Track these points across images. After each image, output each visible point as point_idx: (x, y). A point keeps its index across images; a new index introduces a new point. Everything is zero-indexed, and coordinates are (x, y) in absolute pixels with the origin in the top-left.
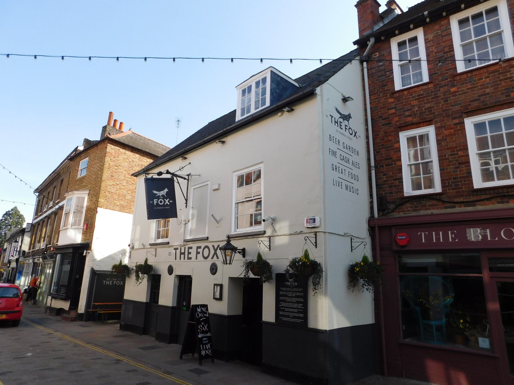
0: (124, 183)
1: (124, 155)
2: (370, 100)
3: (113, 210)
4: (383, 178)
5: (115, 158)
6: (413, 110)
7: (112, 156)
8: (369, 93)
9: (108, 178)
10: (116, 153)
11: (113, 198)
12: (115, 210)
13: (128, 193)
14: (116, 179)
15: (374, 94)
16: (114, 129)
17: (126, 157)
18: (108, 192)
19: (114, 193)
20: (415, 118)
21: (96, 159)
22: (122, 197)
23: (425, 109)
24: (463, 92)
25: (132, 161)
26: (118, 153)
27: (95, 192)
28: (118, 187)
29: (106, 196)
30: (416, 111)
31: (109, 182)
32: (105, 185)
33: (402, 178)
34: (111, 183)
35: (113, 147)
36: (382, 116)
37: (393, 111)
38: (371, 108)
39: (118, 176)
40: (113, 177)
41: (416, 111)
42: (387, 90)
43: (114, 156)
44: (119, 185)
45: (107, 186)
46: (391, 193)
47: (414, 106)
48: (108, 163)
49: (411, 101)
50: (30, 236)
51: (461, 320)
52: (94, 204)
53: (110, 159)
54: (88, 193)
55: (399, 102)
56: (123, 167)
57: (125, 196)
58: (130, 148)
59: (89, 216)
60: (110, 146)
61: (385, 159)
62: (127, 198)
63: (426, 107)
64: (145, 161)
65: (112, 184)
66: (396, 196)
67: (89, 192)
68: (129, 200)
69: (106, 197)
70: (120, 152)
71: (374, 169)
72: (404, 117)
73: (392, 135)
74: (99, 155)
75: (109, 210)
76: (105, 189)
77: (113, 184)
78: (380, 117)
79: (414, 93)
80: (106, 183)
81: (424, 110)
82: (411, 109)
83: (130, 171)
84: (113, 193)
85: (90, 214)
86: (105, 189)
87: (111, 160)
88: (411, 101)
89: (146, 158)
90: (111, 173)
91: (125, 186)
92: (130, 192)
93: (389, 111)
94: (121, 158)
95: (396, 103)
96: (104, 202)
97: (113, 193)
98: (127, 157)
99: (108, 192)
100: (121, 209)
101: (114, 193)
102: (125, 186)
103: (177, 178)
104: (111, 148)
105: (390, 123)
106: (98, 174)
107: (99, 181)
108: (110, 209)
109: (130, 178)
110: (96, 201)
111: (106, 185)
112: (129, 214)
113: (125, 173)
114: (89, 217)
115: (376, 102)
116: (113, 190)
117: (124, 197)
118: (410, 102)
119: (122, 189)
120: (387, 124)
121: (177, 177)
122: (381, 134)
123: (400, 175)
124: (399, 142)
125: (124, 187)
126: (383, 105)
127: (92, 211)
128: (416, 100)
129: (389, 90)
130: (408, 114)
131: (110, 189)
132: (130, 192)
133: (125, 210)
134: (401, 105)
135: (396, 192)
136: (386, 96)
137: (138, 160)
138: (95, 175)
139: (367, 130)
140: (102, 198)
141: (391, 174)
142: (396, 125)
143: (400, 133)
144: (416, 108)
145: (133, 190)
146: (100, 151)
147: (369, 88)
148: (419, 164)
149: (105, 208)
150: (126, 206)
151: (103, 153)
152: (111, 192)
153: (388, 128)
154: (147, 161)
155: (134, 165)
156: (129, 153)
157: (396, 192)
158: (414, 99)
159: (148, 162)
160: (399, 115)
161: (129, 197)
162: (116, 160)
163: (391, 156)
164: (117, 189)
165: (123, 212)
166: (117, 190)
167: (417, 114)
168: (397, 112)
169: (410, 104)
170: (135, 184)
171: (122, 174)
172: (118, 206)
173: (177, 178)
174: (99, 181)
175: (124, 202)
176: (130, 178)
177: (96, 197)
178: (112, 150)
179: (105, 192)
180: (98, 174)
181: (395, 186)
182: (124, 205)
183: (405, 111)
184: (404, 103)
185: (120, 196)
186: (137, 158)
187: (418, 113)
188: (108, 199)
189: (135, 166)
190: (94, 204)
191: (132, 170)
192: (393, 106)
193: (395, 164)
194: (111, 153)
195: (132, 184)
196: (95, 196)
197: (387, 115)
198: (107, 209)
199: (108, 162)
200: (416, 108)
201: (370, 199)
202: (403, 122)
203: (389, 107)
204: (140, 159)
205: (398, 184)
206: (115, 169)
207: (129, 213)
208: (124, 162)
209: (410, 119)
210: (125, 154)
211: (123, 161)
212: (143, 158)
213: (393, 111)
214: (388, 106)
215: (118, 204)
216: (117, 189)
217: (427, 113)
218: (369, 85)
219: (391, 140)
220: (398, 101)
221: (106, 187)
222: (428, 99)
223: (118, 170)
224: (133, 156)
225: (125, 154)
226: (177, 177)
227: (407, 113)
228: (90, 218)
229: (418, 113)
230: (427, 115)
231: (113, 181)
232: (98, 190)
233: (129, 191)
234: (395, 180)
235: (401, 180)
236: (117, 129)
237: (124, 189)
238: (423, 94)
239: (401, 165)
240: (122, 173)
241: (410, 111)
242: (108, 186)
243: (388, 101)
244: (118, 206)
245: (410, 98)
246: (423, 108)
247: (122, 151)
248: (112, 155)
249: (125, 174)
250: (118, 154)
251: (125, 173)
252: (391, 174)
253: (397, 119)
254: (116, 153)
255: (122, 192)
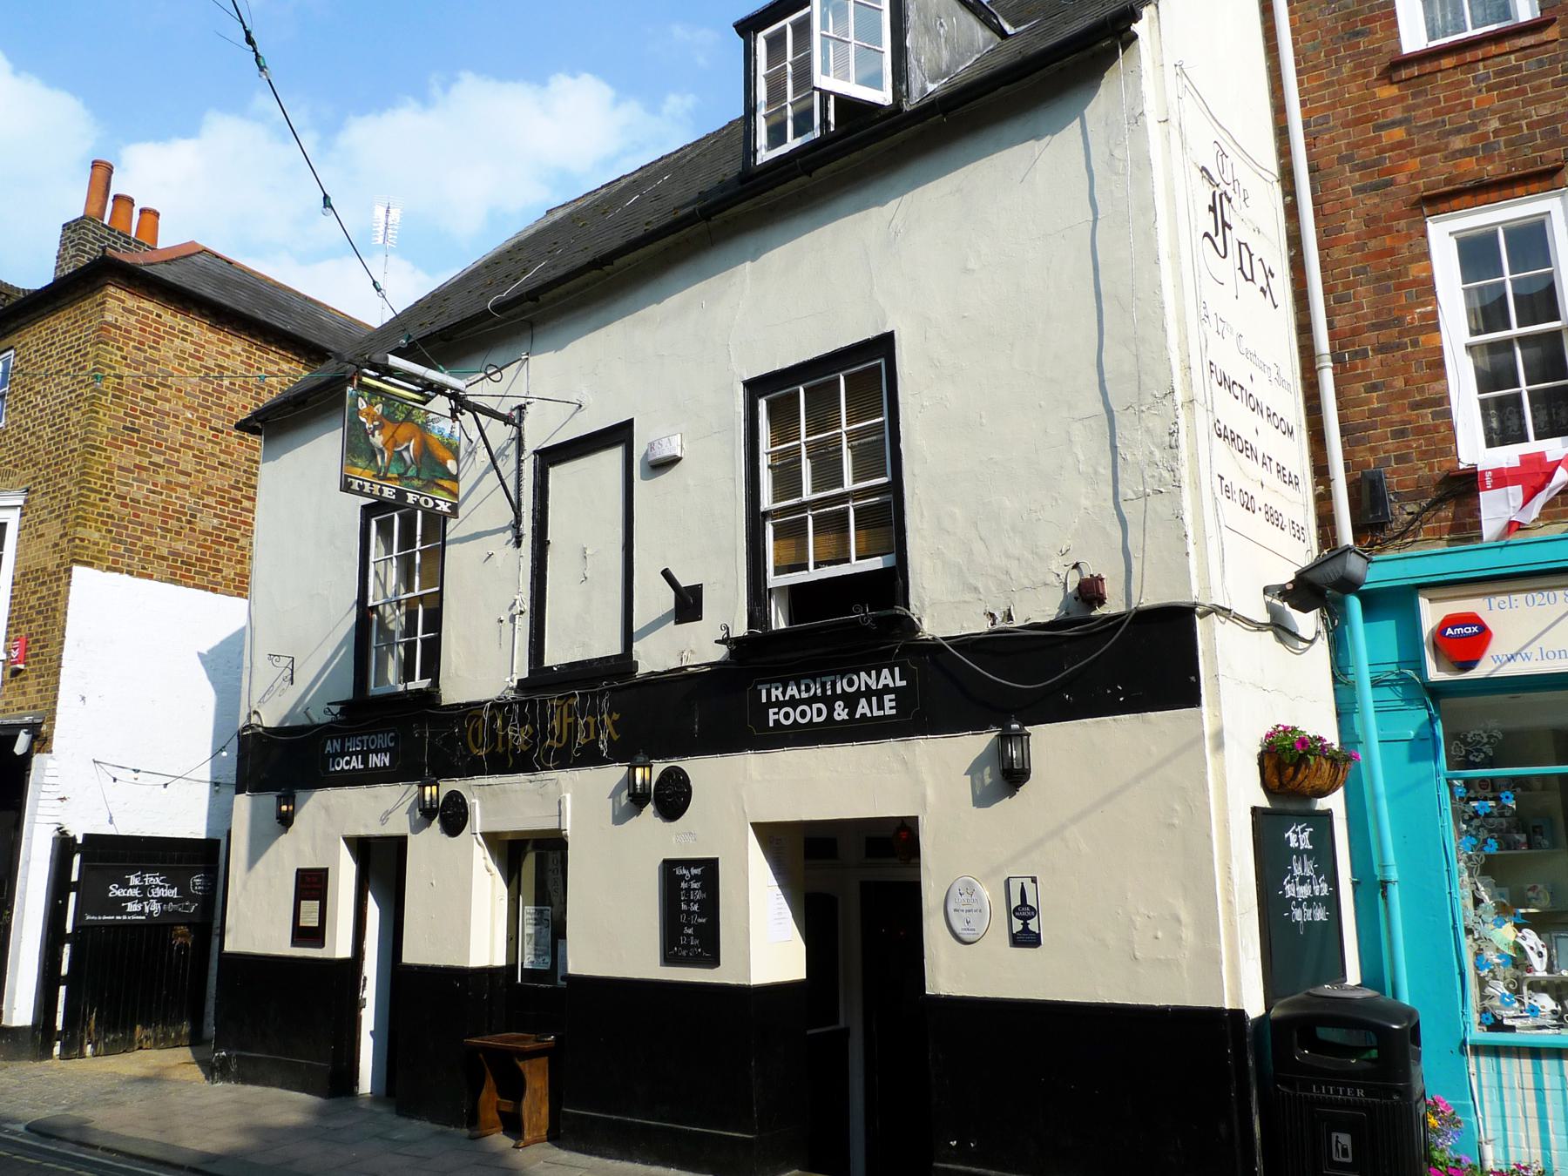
0: (187, 461)
1: (183, 339)
2: (1302, 92)
3: (140, 575)
4: (1368, 401)
5: (145, 352)
6: (1482, 129)
7: (132, 343)
8: (1297, 63)
9: (116, 439)
10: (145, 331)
11: (142, 524)
12: (150, 577)
13: (205, 505)
14: (152, 443)
15: (1315, 68)
16: (114, 236)
17: (190, 348)
18: (117, 496)
19: (145, 503)
20: (1491, 160)
21: (51, 356)
22: (179, 520)
23: (1529, 126)
24: (1455, 126)
25: (217, 369)
26: (157, 329)
27: (55, 497)
28: (161, 479)
29: (111, 517)
30: (1493, 132)
31: (123, 456)
32: (101, 468)
33: (1448, 397)
34: (125, 457)
35: (131, 302)
36: (1353, 154)
37: (1399, 134)
38: (1306, 125)
39: (158, 431)
40: (135, 435)
41: (1493, 132)
42: (1367, 52)
43: (140, 342)
44: (163, 467)
45: (112, 474)
46: (1400, 459)
47: (1483, 113)
48: (112, 372)
49: (1470, 94)
50: (886, 566)
51: (1285, 893)
52: (54, 552)
53: (119, 353)
54: (21, 502)
55: (1420, 100)
56: (180, 391)
57: (192, 516)
58: (207, 313)
59: (32, 603)
60: (119, 299)
61: (1373, 324)
62: (199, 526)
63: (1535, 118)
64: (273, 368)
65: (136, 466)
66: (1427, 470)
67: (26, 501)
68: (210, 534)
69: (110, 521)
70: (162, 328)
71: (1331, 365)
72: (1446, 158)
73: (1397, 231)
74: (68, 340)
75: (125, 576)
76: (105, 486)
77: (137, 462)
78: (1342, 160)
79: (1481, 64)
80: (109, 458)
81: (1525, 127)
82: (1473, 127)
83: (209, 408)
84: (139, 502)
85: (36, 596)
86: (105, 486)
87: (125, 358)
88: (1470, 94)
89: (275, 357)
90: (125, 414)
91: (189, 475)
92: (210, 500)
93: (1380, 136)
94: (167, 350)
95: (1411, 102)
96: (101, 542)
97: (139, 502)
98: (196, 350)
99: (117, 496)
100: (179, 572)
101: (145, 503)
102: (189, 475)
103: (476, 419)
104: (123, 308)
105: (1391, 183)
106: (67, 420)
107: (71, 451)
108: (130, 573)
109: (209, 441)
110: (61, 537)
111: (107, 468)
112: (210, 594)
113: (190, 416)
114: (30, 608)
115: (1323, 98)
116: (139, 488)
117: (189, 522)
118: (1466, 96)
119: (178, 484)
120: (1375, 187)
121: (478, 414)
122: (1353, 226)
123: (1437, 386)
124: (1426, 255)
125: (182, 479)
126: (1355, 110)
127: (44, 583)
128: (1490, 89)
129: (1379, 50)
130: (1462, 146)
131: (126, 484)
132: (210, 500)
133: (193, 578)
134: (1429, 109)
135: (1424, 455)
136: (1366, 75)
137: (242, 362)
138: (50, 427)
139: (1292, 211)
140: (94, 524)
141: (1399, 383)
142: (1415, 189)
143: (1435, 222)
144: (1495, 124)
145: (224, 491)
146: (73, 320)
147: (1294, 46)
148: (1507, 344)
149: (109, 569)
150: (197, 559)
151: (88, 328)
152: (132, 500)
153: (1377, 200)
154: (279, 370)
155: (226, 382)
156: (200, 331)
157: (1424, 455)
158: (1484, 84)
159: (283, 372)
160: (1425, 152)
161: (207, 521)
162: (145, 358)
163: (1396, 314)
164: (155, 485)
165: (186, 585)
166: (154, 492)
167: (1496, 146)
168: (1413, 139)
169: (1467, 106)
170: (231, 467)
171: (177, 423)
172: (164, 558)
173: (476, 419)
174: (71, 451)
175: (191, 543)
176: (209, 441)
177: (63, 521)
178: (128, 315)
179: (103, 496)
180: (67, 420)
181: (1420, 431)
182: (189, 557)
183: (1449, 135)
184: (1442, 104)
185: (171, 517)
186: (239, 355)
187: (1502, 143)
188: (118, 526)
189: (231, 390)
190: (54, 552)
191: (218, 405)
192: (1397, 113)
193: (1415, 343)
194: (126, 331)
195: (221, 464)
196: (58, 516)
197: (1374, 150)
198: (115, 570)
199: (113, 368)
200: (1491, 122)
201: (1317, 484)
202: (1443, 177)
203: (1381, 121)
204: (252, 362)
205: (1429, 420)
206: (143, 399)
207: (214, 590)
208: (180, 371)
209: (1470, 165)
210: (187, 334)
211: (179, 364)
212: (262, 357)
213: (1399, 134)
214: (1378, 114)
215: (165, 552)
216: (155, 485)
217: (1539, 141)
218: (1295, 31)
219: (1393, 249)
220: (1414, 95)
221: (106, 476)
222: (1540, 88)
223: (159, 402)
224: (221, 344)
225: (187, 334)
226: (478, 414)
227: (1458, 143)
228: (38, 613)
229: (1502, 143)
230: (1535, 149)
231: (137, 452)
232: (70, 492)
233: (208, 494)
234: (1417, 406)
235: (1441, 404)
236: (129, 238)
237: (187, 487)
238: (1519, 69)
239: (1441, 350)
240: (176, 417)
241: (1469, 135)
242: (116, 472)
243: (1374, 93)
244: (164, 558)
245: (1466, 83)
246: (1524, 123)
247: (171, 318)
248: (131, 339)
249: (191, 421)
250: (154, 335)
251: (190, 416)
252: (1399, 383)
253: (1415, 164)
254: (145, 331)
255: (177, 498)
